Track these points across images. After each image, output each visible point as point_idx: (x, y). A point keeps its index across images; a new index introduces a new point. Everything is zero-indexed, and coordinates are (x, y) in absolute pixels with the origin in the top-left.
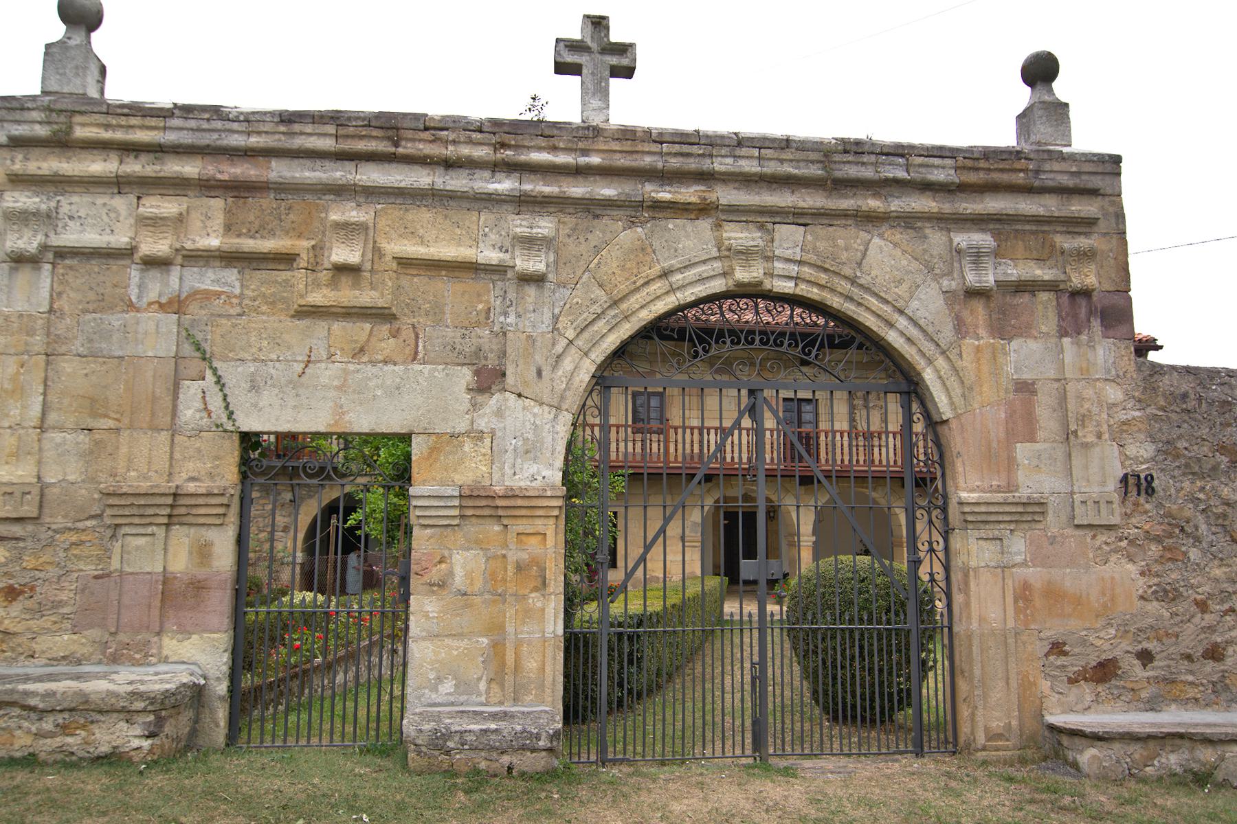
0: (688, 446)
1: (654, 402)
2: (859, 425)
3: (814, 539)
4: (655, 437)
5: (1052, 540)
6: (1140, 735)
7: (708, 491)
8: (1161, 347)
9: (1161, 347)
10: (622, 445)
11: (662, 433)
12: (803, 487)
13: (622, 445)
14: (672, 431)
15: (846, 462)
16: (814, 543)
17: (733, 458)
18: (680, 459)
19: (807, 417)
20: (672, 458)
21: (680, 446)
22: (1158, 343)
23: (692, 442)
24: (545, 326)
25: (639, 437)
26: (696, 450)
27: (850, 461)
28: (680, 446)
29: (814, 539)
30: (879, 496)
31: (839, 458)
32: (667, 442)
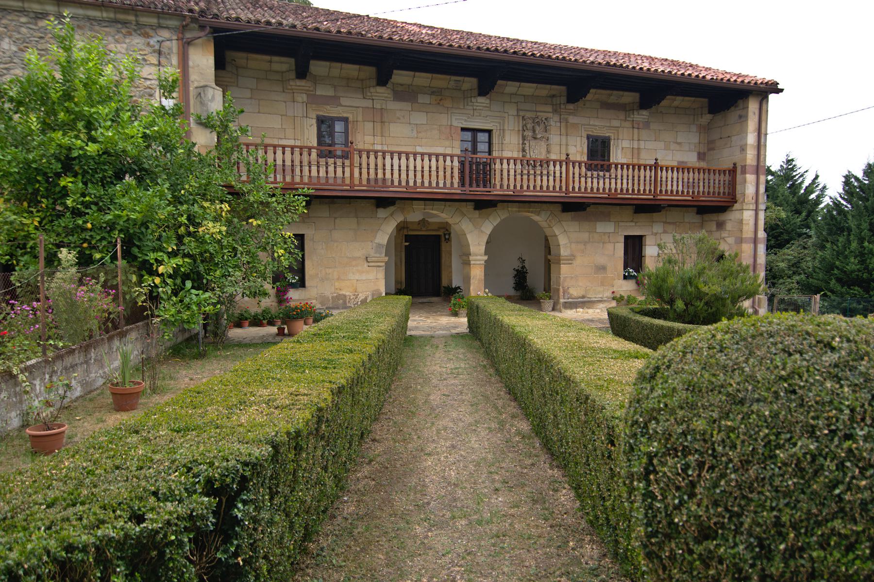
0: (372, 171)
1: (339, 127)
2: (528, 154)
3: (486, 258)
4: (339, 162)
5: (789, 290)
6: (78, 5)
7: (392, 215)
8: (781, 90)
9: (781, 90)
10: (306, 169)
11: (347, 158)
12: (477, 212)
13: (306, 169)
14: (356, 157)
15: (518, 188)
16: (486, 261)
17: (415, 182)
18: (364, 182)
19: (482, 147)
20: (357, 182)
21: (364, 171)
22: (780, 87)
23: (376, 165)
24: (624, 491)
25: (322, 161)
26: (380, 176)
27: (522, 187)
28: (364, 171)
29: (486, 258)
30: (540, 218)
31: (505, 183)
32: (352, 166)
